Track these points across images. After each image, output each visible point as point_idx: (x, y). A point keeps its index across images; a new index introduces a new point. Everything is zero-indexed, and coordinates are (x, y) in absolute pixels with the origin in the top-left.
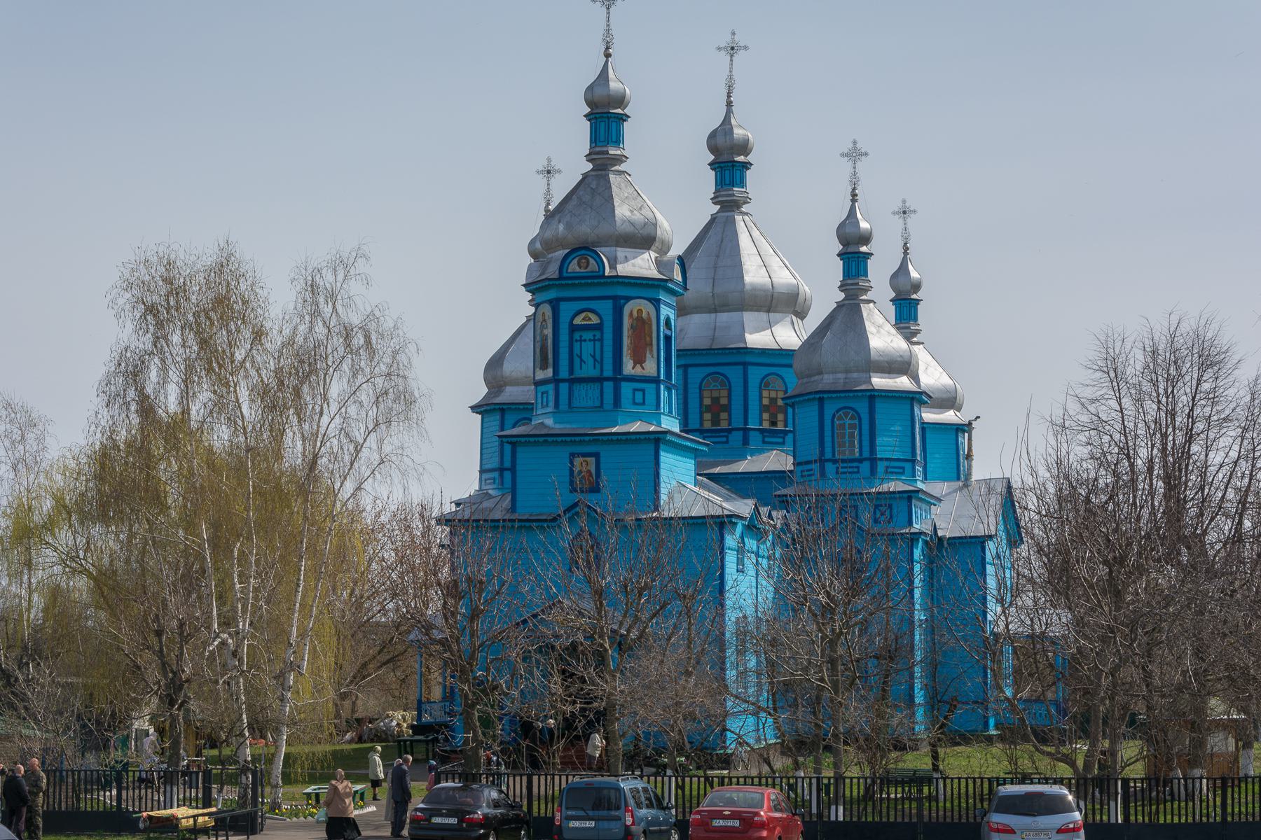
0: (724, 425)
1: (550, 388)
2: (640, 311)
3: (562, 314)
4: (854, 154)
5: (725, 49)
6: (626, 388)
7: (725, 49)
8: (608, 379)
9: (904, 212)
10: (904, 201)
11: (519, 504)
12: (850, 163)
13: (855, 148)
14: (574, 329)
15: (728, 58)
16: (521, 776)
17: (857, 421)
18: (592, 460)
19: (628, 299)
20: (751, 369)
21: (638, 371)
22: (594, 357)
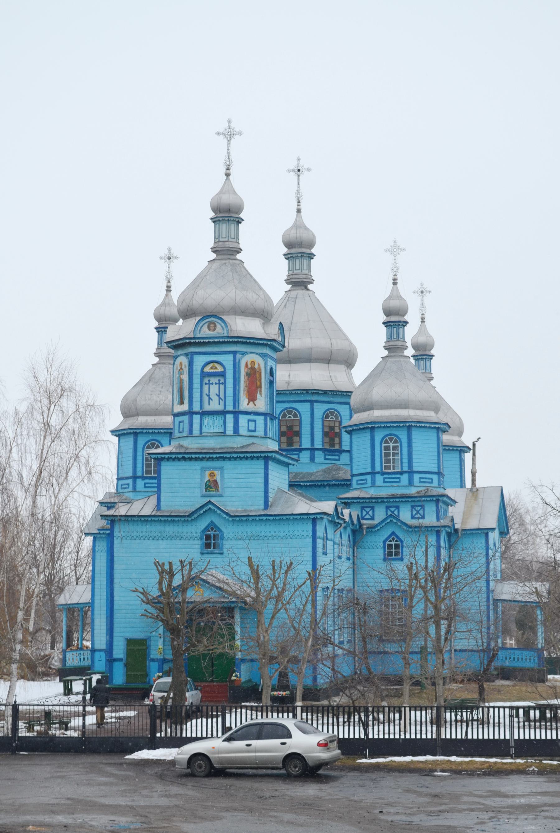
0: (296, 447)
1: (186, 418)
2: (253, 363)
4: (395, 250)
5: (304, 170)
6: (243, 420)
7: (293, 171)
8: (229, 412)
9: (422, 292)
10: (422, 284)
11: (162, 503)
12: (392, 257)
13: (395, 245)
14: (204, 375)
15: (296, 177)
16: (431, 708)
19: (244, 354)
20: (316, 405)
21: (251, 407)
22: (219, 396)
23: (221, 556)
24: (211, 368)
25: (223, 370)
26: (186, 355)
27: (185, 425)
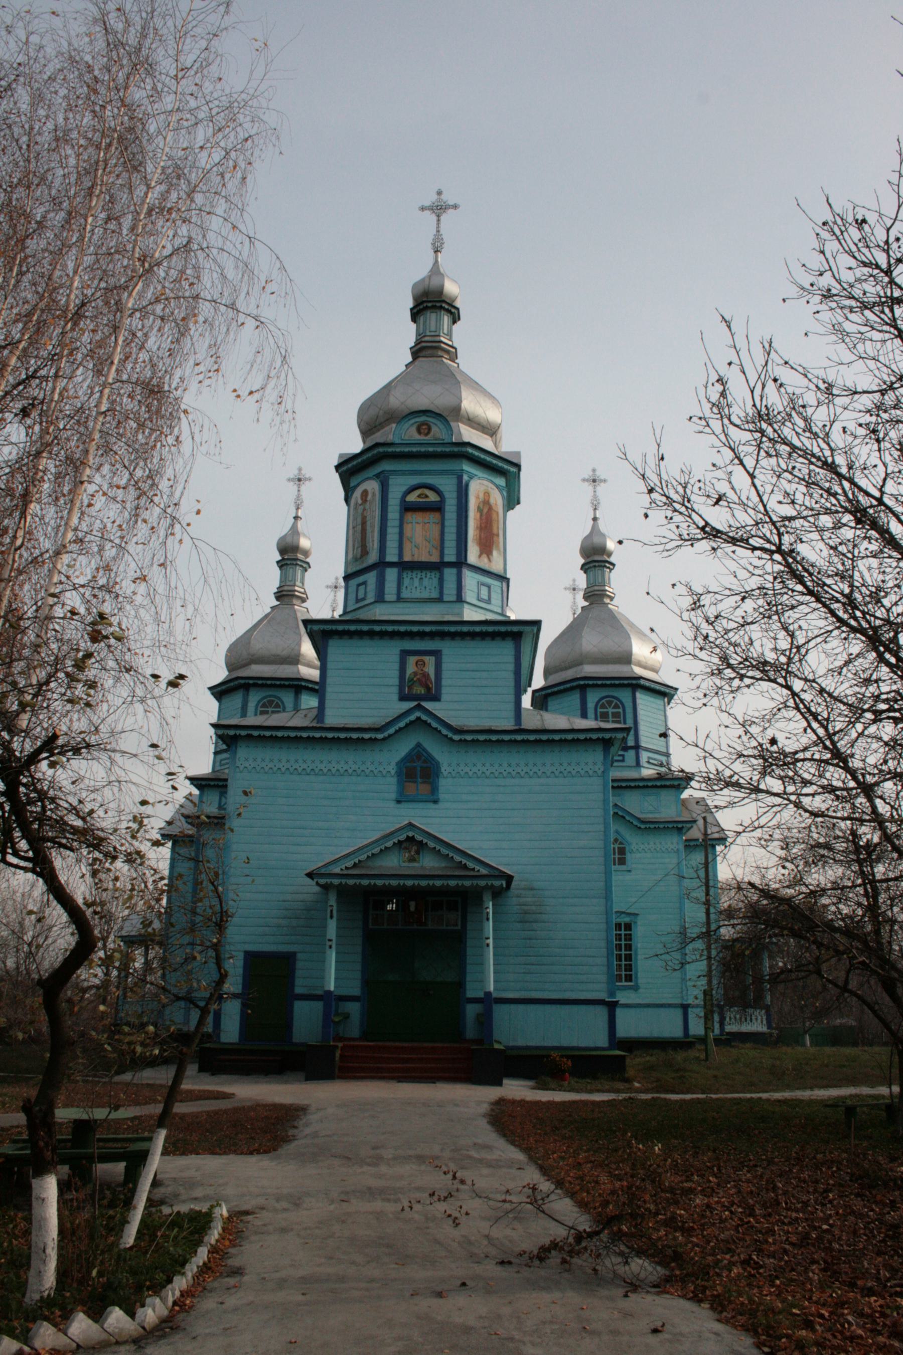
3: (391, 489)
14: (408, 508)
17: (621, 710)
18: (430, 661)
21: (484, 563)
23: (436, 806)
24: (419, 496)
25: (438, 499)
26: (377, 476)
27: (369, 589)
